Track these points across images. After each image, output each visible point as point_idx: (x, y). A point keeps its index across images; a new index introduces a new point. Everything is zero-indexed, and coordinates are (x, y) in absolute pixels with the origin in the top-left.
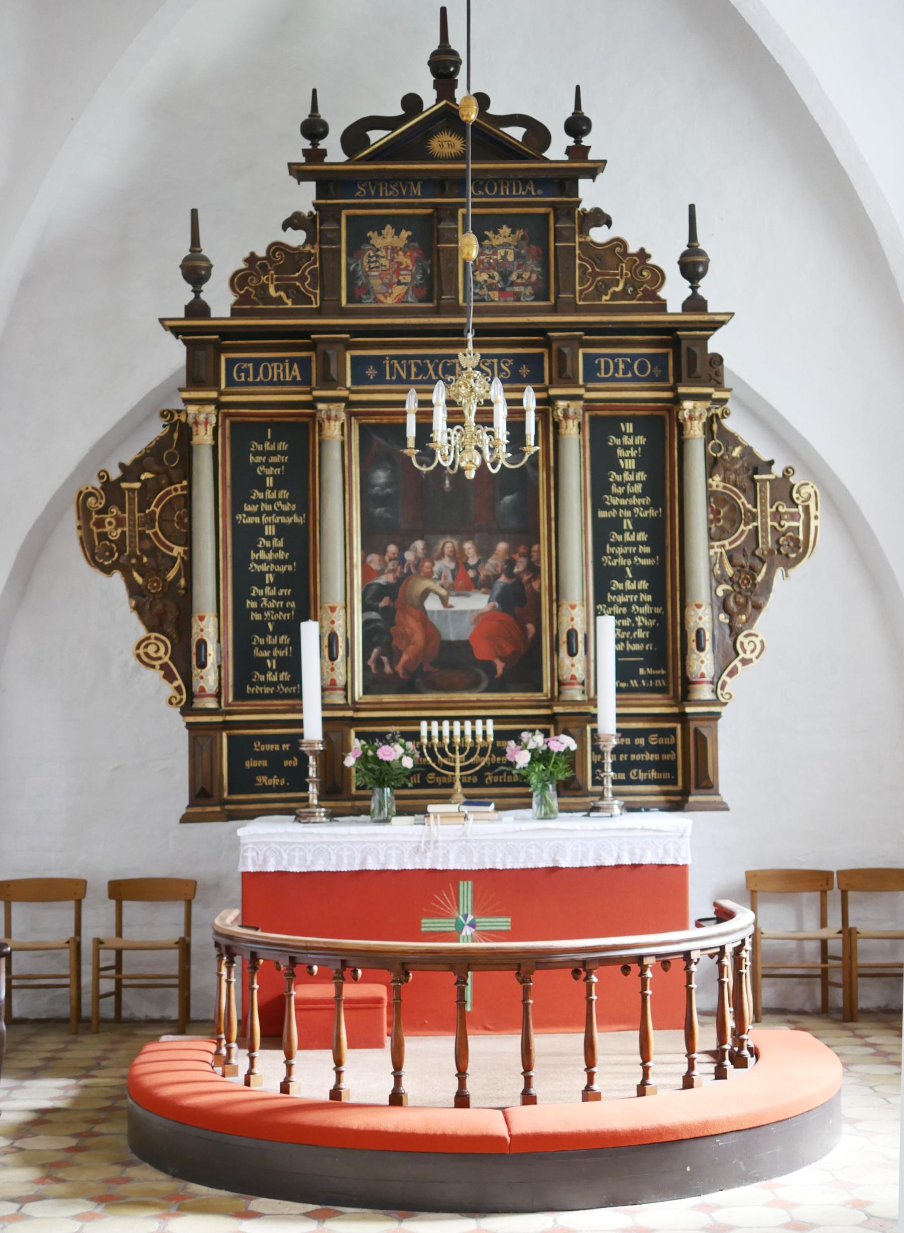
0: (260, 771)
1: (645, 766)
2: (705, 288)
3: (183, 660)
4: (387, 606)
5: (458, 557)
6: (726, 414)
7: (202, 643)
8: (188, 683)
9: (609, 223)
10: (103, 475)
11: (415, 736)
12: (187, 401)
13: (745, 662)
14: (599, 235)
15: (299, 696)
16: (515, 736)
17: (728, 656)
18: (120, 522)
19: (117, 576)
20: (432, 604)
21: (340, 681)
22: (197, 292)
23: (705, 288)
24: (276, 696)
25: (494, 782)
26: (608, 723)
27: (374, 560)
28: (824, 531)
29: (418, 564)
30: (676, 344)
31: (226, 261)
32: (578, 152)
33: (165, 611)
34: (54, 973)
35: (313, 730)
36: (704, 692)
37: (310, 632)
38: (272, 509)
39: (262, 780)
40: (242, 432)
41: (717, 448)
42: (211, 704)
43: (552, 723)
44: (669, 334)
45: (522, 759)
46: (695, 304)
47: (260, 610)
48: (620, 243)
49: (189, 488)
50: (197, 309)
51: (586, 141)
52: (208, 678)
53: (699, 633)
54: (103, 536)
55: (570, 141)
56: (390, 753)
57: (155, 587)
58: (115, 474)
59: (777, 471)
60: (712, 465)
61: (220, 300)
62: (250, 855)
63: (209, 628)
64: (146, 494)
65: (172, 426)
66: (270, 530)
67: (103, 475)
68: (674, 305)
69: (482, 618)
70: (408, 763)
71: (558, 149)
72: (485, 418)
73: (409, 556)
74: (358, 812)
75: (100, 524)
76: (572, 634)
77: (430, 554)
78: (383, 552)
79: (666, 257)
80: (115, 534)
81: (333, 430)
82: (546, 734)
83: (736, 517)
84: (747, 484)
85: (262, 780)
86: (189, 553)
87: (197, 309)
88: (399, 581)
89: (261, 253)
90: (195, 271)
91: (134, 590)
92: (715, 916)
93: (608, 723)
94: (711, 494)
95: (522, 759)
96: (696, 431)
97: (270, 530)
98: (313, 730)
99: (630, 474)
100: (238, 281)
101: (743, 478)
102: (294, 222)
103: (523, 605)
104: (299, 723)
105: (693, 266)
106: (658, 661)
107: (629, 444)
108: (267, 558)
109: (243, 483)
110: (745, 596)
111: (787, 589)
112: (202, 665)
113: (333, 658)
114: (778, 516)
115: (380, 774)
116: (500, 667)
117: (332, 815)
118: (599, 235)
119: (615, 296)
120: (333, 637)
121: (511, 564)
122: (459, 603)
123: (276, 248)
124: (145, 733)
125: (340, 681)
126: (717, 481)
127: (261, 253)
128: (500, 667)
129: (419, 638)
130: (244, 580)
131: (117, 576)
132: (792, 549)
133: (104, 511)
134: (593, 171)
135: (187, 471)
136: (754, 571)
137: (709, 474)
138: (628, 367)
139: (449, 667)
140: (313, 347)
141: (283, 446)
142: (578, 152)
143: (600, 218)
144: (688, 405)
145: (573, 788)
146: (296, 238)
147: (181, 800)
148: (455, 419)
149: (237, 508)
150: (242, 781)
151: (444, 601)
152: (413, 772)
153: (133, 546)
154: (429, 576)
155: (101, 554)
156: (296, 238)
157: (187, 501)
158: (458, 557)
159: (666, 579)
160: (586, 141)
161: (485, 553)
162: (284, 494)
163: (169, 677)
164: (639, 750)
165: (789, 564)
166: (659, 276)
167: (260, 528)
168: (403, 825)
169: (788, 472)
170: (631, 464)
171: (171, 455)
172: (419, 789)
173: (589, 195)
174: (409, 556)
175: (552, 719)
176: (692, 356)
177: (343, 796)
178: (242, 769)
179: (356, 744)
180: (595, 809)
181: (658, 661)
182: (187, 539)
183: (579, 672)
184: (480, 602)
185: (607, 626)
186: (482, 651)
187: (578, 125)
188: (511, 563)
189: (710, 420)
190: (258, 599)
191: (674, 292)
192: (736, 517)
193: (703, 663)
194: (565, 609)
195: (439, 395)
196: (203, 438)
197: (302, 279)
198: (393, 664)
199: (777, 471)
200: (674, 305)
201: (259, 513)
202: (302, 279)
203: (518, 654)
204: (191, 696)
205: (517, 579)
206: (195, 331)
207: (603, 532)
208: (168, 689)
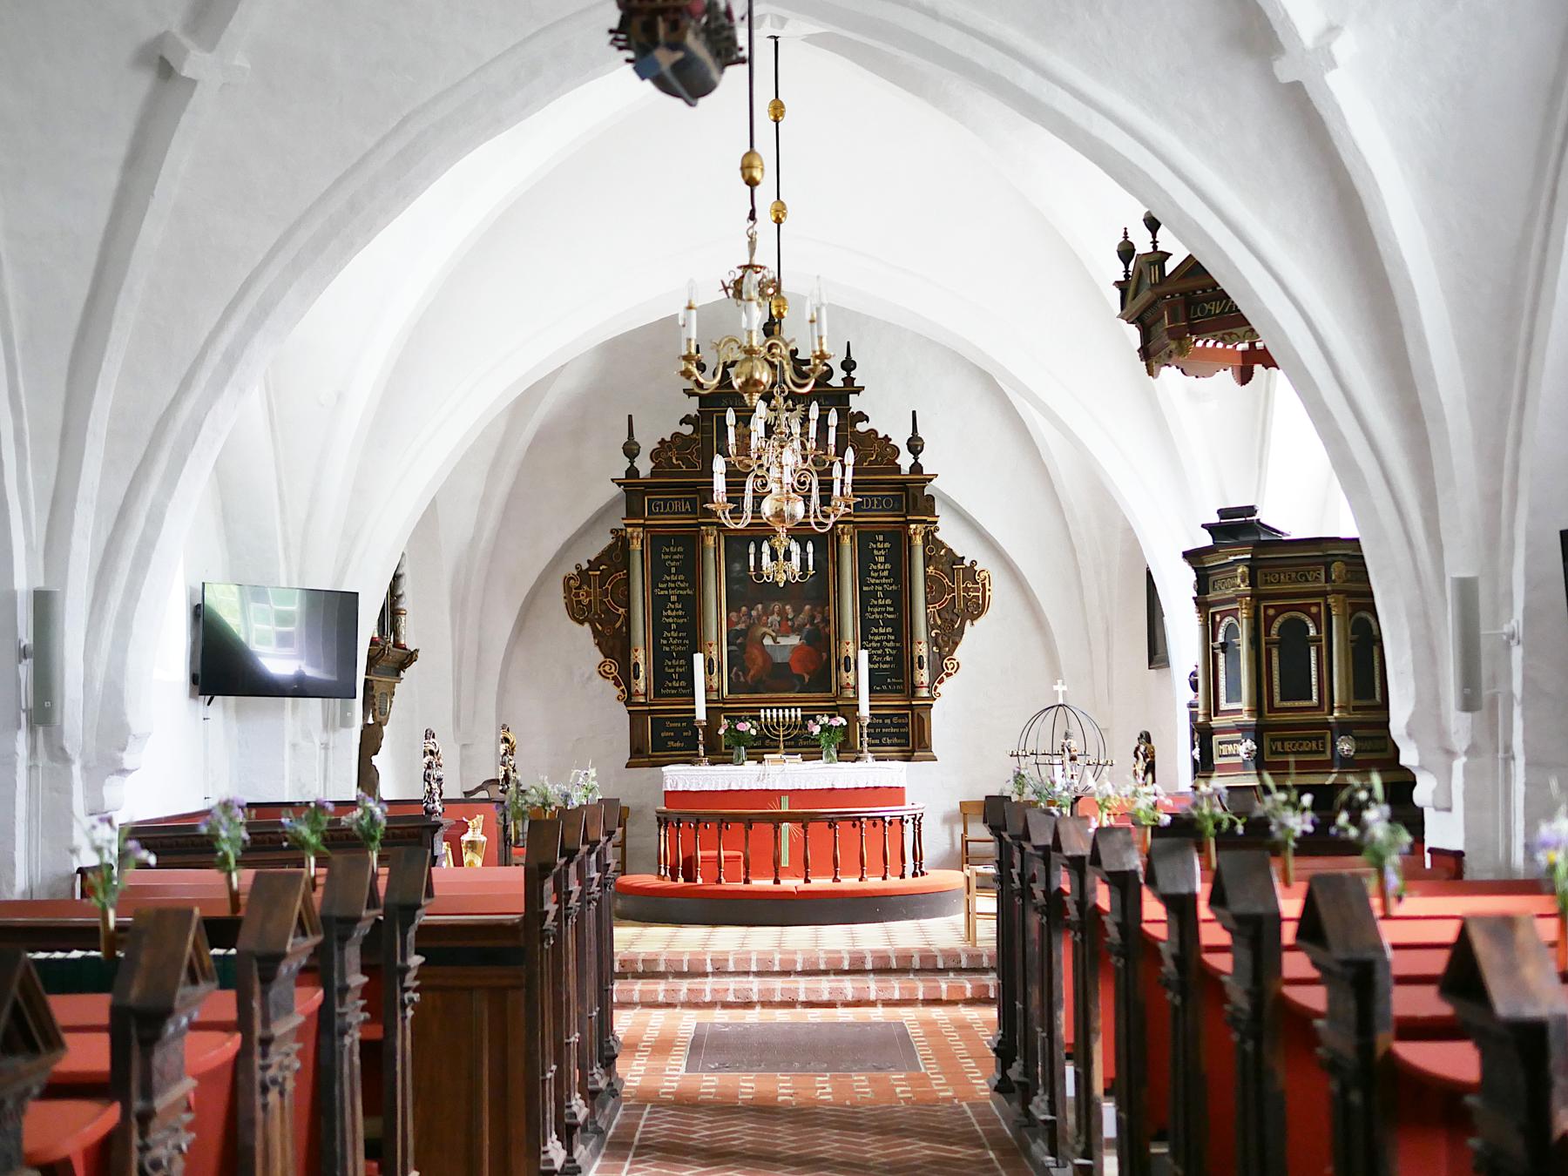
0: (670, 738)
1: (891, 735)
2: (922, 459)
3: (625, 675)
4: (741, 643)
5: (782, 613)
6: (937, 529)
7: (637, 664)
8: (629, 687)
9: (867, 419)
10: (578, 567)
11: (758, 718)
12: (627, 525)
13: (948, 675)
14: (862, 427)
15: (693, 695)
16: (813, 718)
17: (938, 674)
18: (588, 595)
19: (587, 625)
20: (768, 641)
21: (715, 686)
22: (632, 463)
23: (922, 459)
24: (677, 695)
25: (803, 745)
26: (864, 711)
27: (734, 615)
28: (999, 592)
29: (759, 617)
30: (906, 490)
31: (647, 442)
32: (849, 381)
33: (615, 646)
34: (1311, 314)
35: (701, 714)
36: (924, 693)
37: (699, 659)
38: (674, 587)
39: (671, 743)
40: (658, 541)
41: (931, 550)
42: (642, 700)
43: (833, 711)
44: (903, 485)
45: (816, 730)
46: (916, 468)
47: (668, 645)
48: (874, 432)
49: (628, 574)
50: (632, 472)
51: (853, 374)
52: (641, 685)
53: (920, 657)
54: (579, 602)
55: (844, 374)
56: (744, 727)
57: (608, 632)
58: (585, 566)
59: (967, 563)
60: (928, 561)
61: (644, 466)
62: (669, 782)
63: (640, 656)
64: (603, 578)
65: (617, 538)
66: (673, 598)
67: (578, 567)
68: (905, 469)
69: (795, 649)
70: (753, 732)
71: (836, 381)
72: (788, 556)
73: (754, 613)
74: (725, 763)
75: (577, 595)
76: (847, 658)
77: (767, 612)
78: (739, 611)
79: (900, 440)
80: (586, 602)
81: (710, 541)
82: (831, 717)
83: (943, 590)
84: (949, 571)
85: (671, 743)
86: (628, 612)
87: (632, 472)
88: (748, 628)
89: (668, 439)
90: (631, 450)
91: (596, 633)
92: (1315, 974)
93: (864, 711)
94: (927, 577)
95: (816, 730)
96: (918, 541)
97: (673, 598)
98: (701, 714)
99: (882, 565)
100: (654, 455)
101: (947, 568)
102: (686, 420)
103: (821, 642)
104: (694, 711)
105: (915, 445)
106: (895, 675)
107: (880, 548)
108: (672, 615)
109: (658, 572)
110: (948, 638)
111: (973, 633)
112: (637, 677)
113: (711, 673)
114: (967, 590)
115: (738, 738)
116: (807, 678)
117: (713, 763)
118: (862, 427)
119: (871, 463)
120: (711, 660)
121: (813, 617)
122: (783, 641)
123: (676, 435)
124: (606, 718)
125: (715, 686)
126: (931, 569)
127: (668, 439)
128: (807, 678)
129: (760, 661)
130: (659, 628)
131: (587, 625)
132: (976, 609)
133: (579, 588)
134: (858, 391)
135: (627, 565)
136: (953, 622)
137: (926, 566)
138: (880, 502)
139: (777, 679)
140: (698, 492)
141: (680, 549)
142: (849, 381)
143: (862, 417)
144: (913, 526)
145: (847, 750)
146: (687, 430)
147: (626, 755)
148: (774, 556)
149: (655, 586)
150: (659, 744)
151: (774, 640)
152: (756, 738)
153: (596, 607)
154: (765, 625)
155: (578, 612)
156: (687, 430)
157: (627, 582)
158: (782, 613)
159: (902, 628)
160: (853, 374)
161: (797, 612)
162: (682, 577)
163: (617, 684)
164: (884, 726)
165: (974, 618)
166: (896, 451)
167: (669, 596)
168: (751, 766)
169: (973, 563)
170: (882, 559)
171: (618, 553)
172: (760, 747)
173: (856, 403)
174: (754, 613)
175: (836, 708)
176: (915, 498)
177: (719, 753)
178: (661, 735)
179: (725, 722)
180: (858, 759)
181: (895, 675)
182: (627, 605)
183: (852, 681)
184: (794, 640)
185: (864, 655)
186: (796, 669)
187: (848, 365)
188: (813, 617)
189: (927, 534)
190: (667, 638)
191: (905, 461)
192: (943, 590)
193: (923, 676)
194: (843, 644)
195: (765, 548)
196: (636, 546)
197: (691, 454)
198: (745, 675)
199: (967, 563)
200: (905, 469)
201: (667, 589)
202: (691, 454)
203: (818, 673)
204: (630, 697)
205: (817, 626)
206: (631, 484)
207: (865, 600)
208: (617, 691)
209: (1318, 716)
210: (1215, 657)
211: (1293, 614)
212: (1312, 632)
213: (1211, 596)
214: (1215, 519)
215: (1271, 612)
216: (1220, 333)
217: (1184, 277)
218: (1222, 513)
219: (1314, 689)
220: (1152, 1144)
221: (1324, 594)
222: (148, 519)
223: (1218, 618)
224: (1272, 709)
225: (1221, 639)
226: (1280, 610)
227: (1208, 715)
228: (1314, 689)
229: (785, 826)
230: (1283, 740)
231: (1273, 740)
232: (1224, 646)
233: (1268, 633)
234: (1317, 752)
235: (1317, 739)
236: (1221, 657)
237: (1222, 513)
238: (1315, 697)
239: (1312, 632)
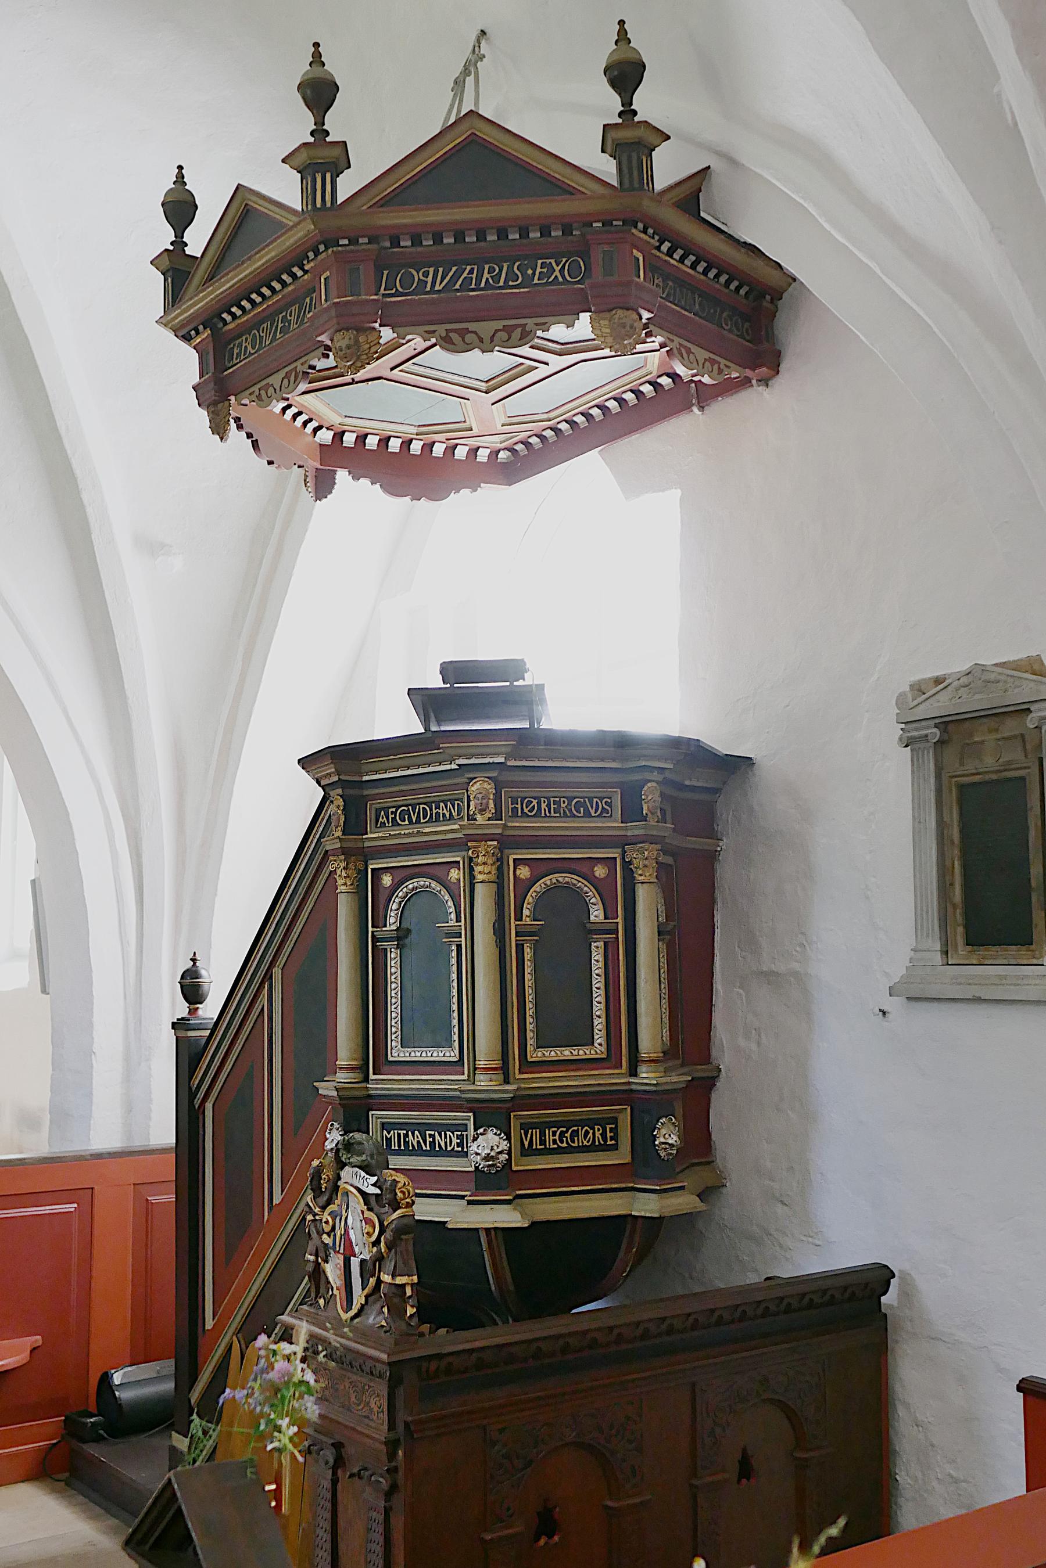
209: (615, 1078)
210: (381, 957)
211: (563, 878)
212: (597, 914)
213: (374, 836)
214: (435, 681)
215: (524, 872)
216: (441, 330)
217: (386, 202)
218: (448, 670)
219: (599, 1024)
220: (40, 1343)
221: (623, 843)
222: (1001, 977)
223: (387, 880)
224: (526, 1065)
225: (392, 922)
226: (541, 868)
227: (363, 1068)
228: (599, 1024)
229: (473, 286)
230: (543, 1127)
231: (525, 1127)
232: (402, 936)
233: (519, 917)
234: (604, 1148)
235: (602, 1122)
236: (393, 958)
237: (448, 670)
238: (600, 1037)
239: (597, 914)
